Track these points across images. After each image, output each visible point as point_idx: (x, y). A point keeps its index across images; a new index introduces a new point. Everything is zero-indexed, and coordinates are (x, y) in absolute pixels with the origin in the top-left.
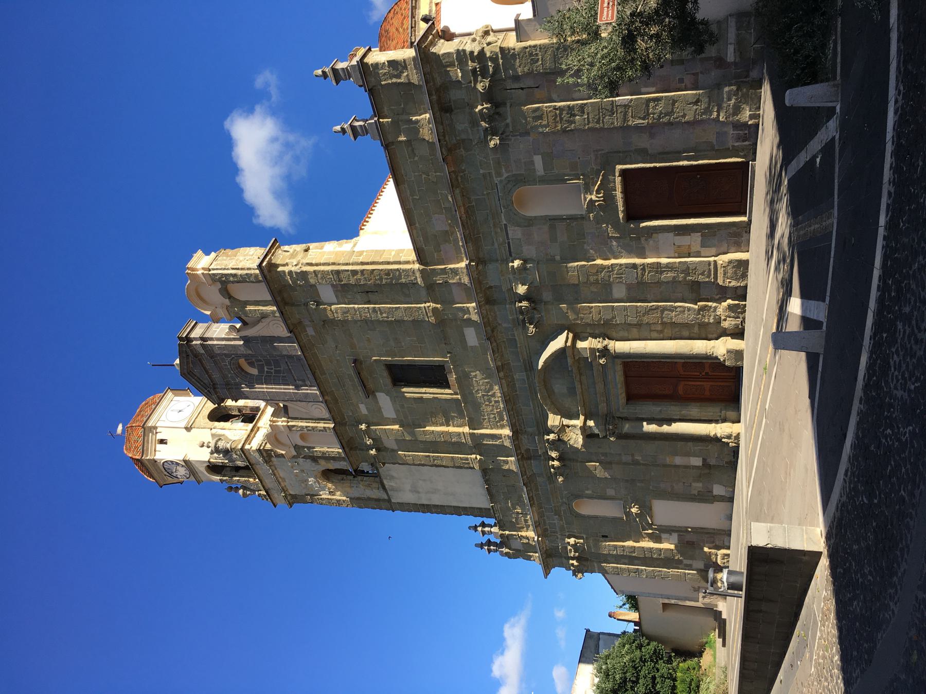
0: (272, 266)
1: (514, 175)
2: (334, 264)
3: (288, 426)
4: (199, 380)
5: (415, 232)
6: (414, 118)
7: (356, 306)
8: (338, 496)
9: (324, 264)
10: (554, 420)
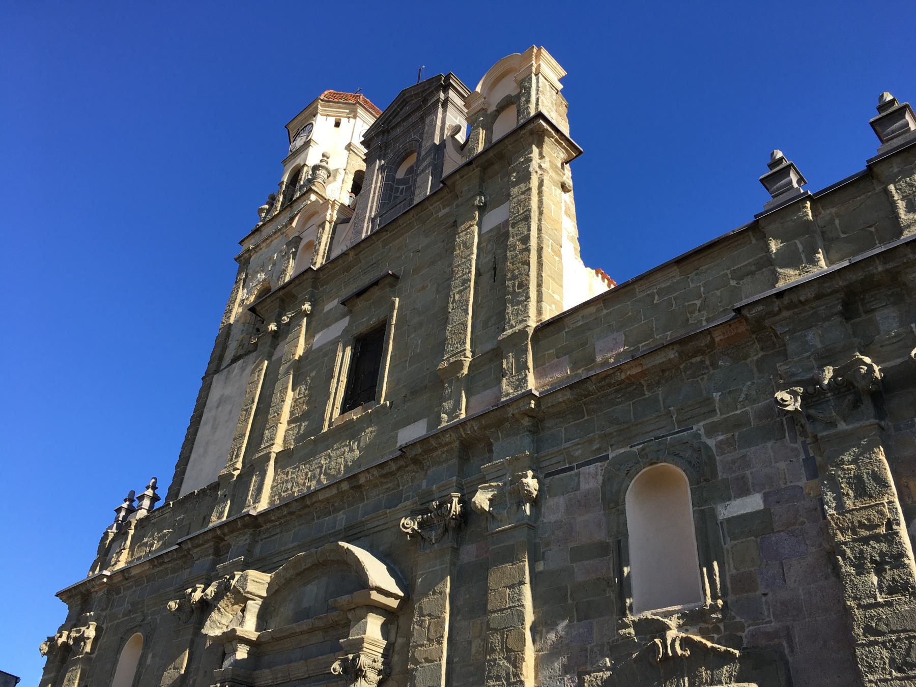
0: (539, 138)
1: (711, 458)
2: (541, 213)
3: (324, 222)
4: (395, 114)
5: (592, 309)
6: (820, 256)
7: (474, 257)
8: (237, 310)
9: (541, 202)
10: (258, 582)
